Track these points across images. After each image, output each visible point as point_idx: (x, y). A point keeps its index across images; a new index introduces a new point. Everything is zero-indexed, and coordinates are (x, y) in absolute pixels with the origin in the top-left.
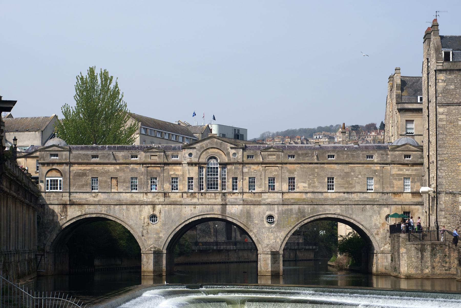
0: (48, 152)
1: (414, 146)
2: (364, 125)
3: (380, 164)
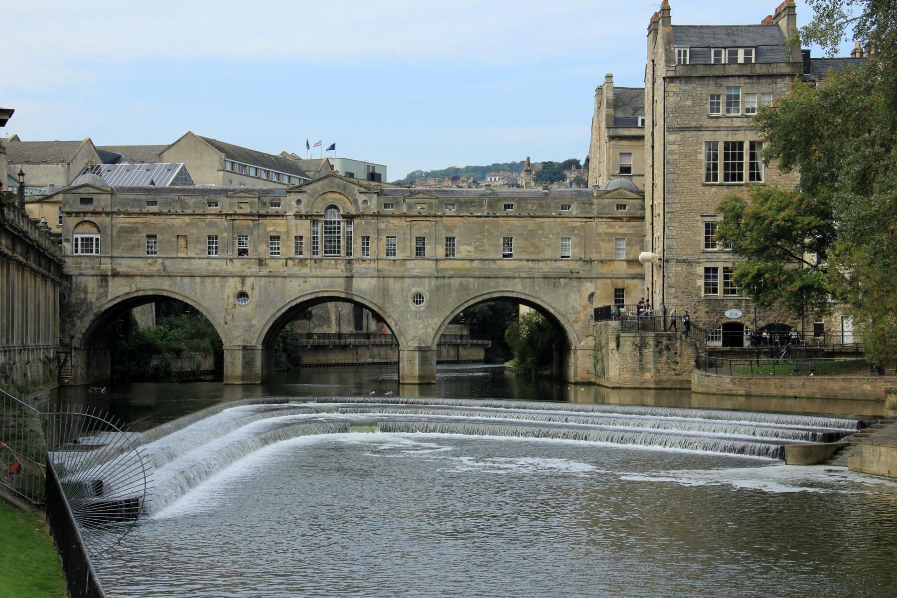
2: (561, 161)
3: (581, 218)
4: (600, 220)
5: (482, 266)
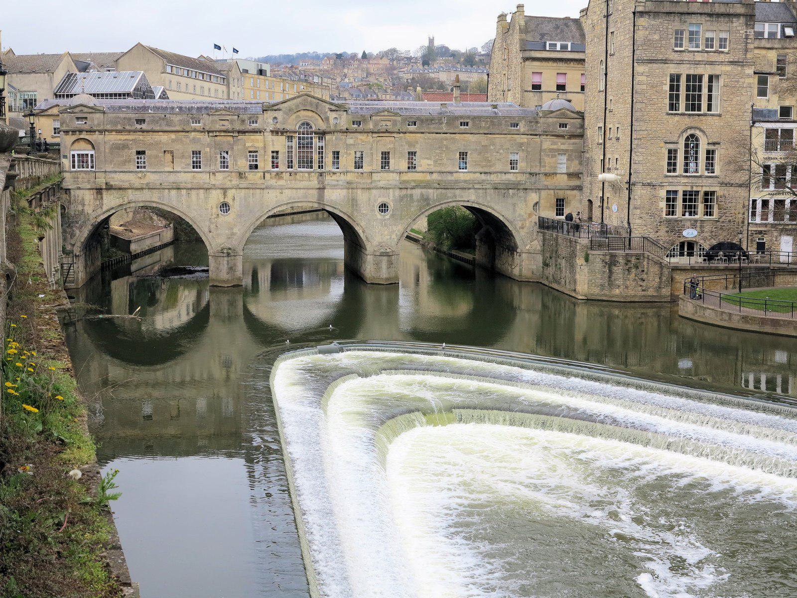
0: (72, 114)
1: (572, 112)
4: (545, 137)
5: (440, 178)
